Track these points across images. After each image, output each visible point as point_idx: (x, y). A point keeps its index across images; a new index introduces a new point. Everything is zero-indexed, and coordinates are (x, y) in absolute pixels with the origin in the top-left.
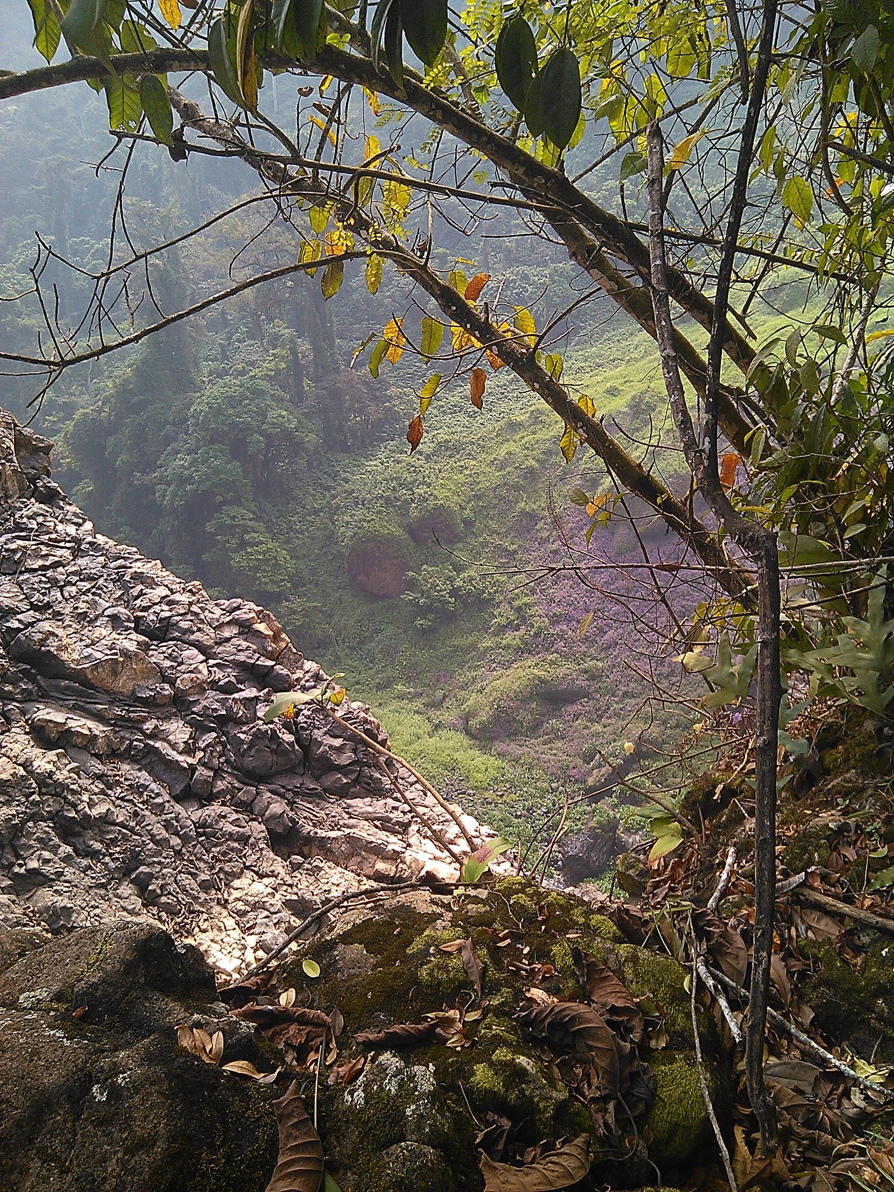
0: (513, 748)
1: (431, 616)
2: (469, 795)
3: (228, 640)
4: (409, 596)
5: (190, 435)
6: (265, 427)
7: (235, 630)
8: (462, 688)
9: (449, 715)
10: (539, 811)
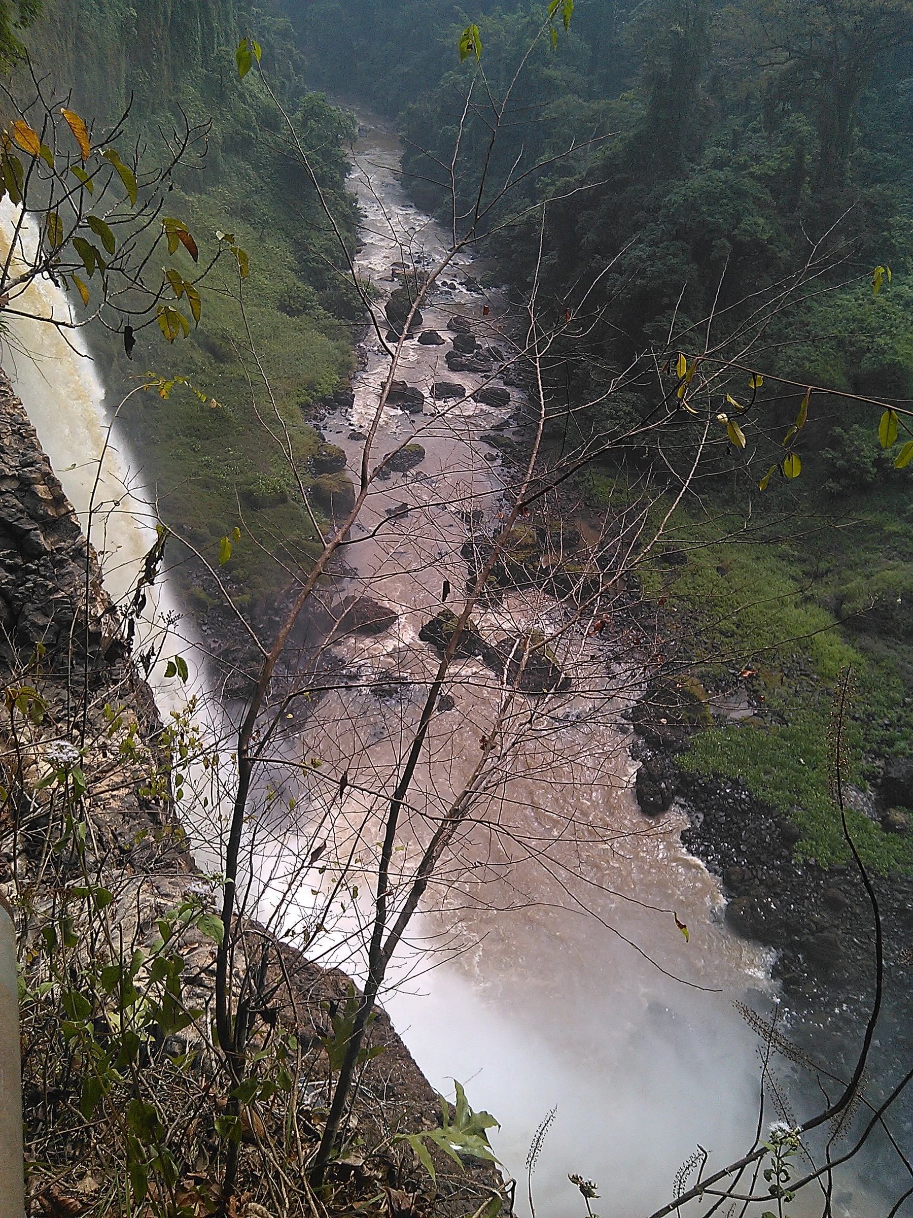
0: (879, 647)
1: (844, 482)
2: (812, 679)
4: (828, 454)
5: (657, 225)
7: (15, 485)
8: (850, 567)
9: (824, 591)
10: (880, 721)
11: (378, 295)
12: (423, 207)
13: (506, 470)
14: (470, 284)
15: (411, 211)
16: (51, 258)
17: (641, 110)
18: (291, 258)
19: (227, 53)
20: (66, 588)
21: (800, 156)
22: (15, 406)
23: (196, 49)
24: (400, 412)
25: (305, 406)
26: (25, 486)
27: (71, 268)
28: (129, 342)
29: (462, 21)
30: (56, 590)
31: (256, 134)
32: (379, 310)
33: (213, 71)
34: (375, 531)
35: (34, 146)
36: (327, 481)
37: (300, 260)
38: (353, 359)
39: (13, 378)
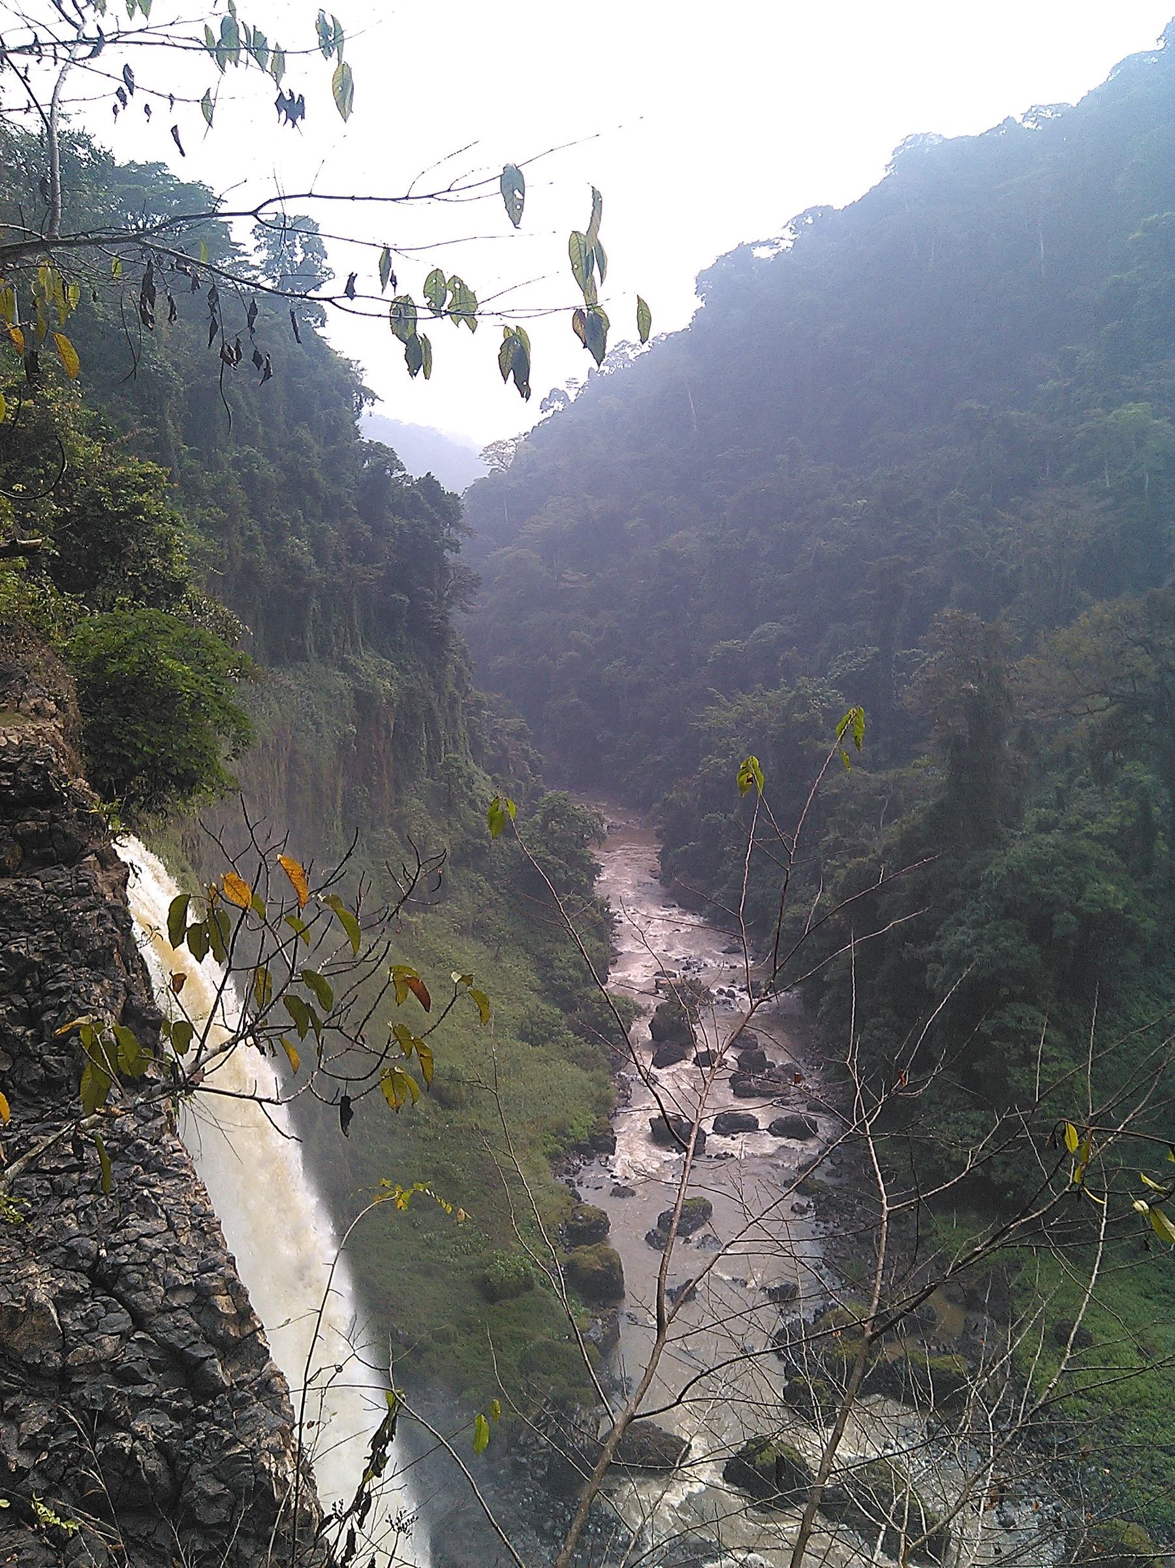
3: (173, 1310)
6: (1081, 903)
7: (190, 1297)
11: (641, 1012)
12: (689, 906)
13: (822, 1225)
14: (752, 989)
15: (675, 911)
16: (257, 1022)
17: (940, 776)
18: (533, 977)
19: (456, 760)
20: (247, 1439)
21: (1145, 810)
22: (197, 1193)
23: (421, 761)
24: (676, 1156)
25: (553, 1157)
26: (203, 1298)
27: (281, 1031)
28: (346, 1115)
29: (719, 703)
30: (233, 1442)
31: (489, 843)
32: (642, 1030)
33: (440, 779)
34: (681, 1396)
35: (245, 897)
36: (587, 1256)
37: (543, 978)
38: (612, 1092)
39: (197, 1155)
